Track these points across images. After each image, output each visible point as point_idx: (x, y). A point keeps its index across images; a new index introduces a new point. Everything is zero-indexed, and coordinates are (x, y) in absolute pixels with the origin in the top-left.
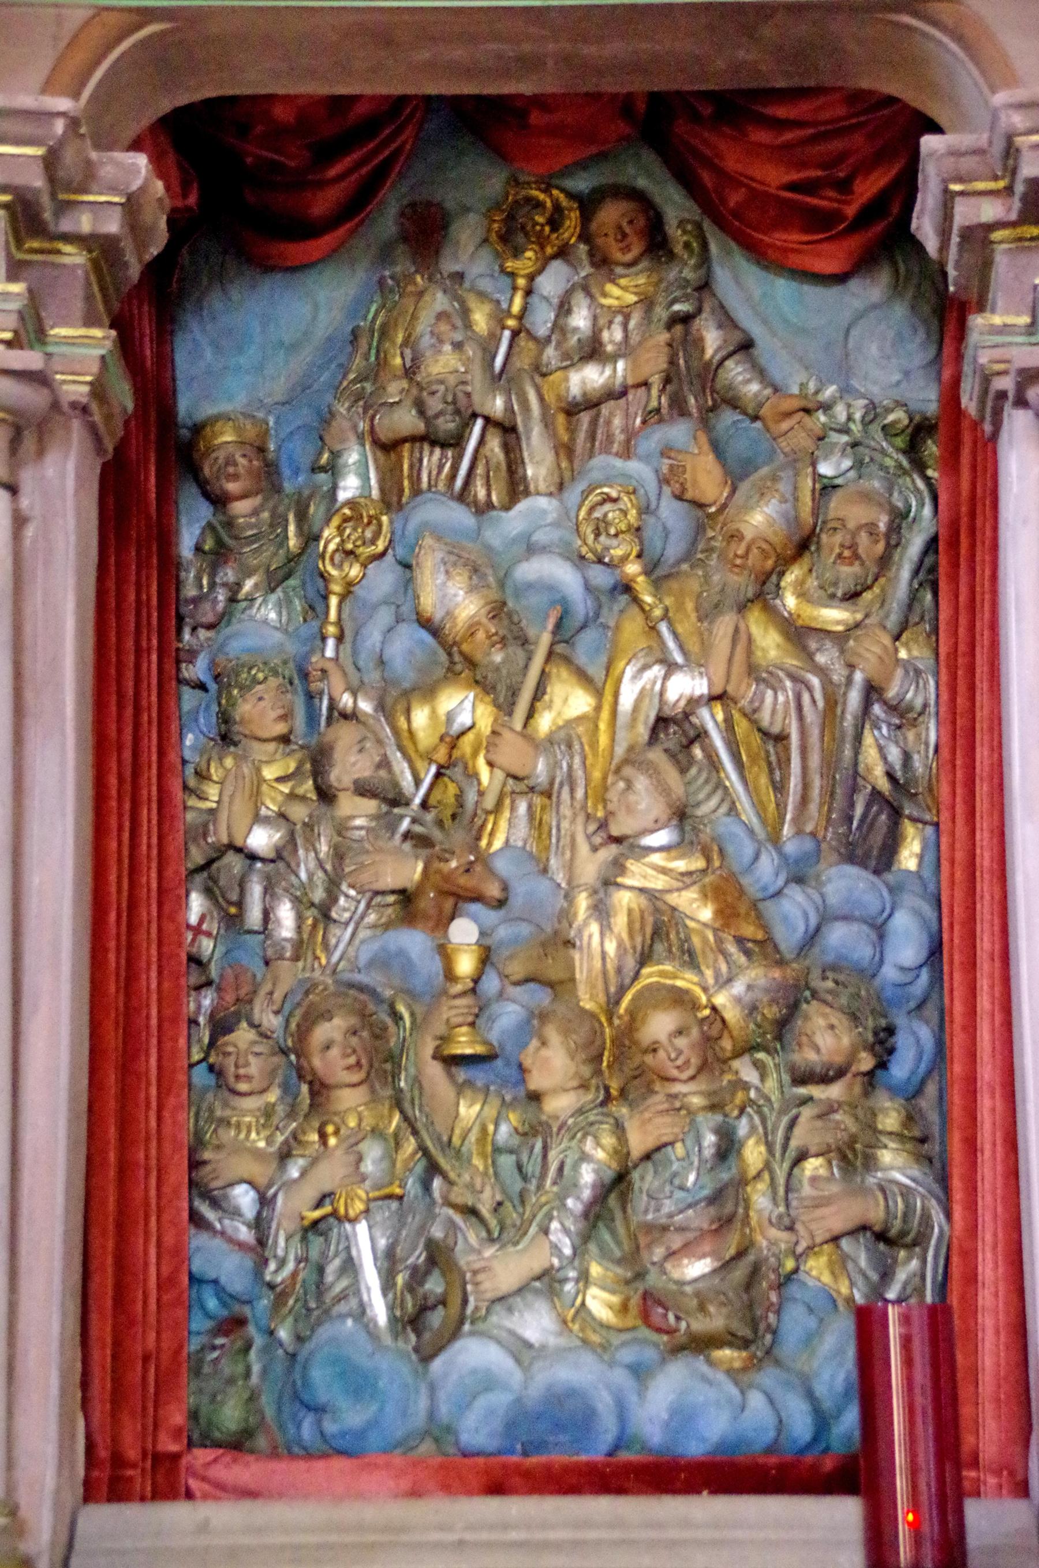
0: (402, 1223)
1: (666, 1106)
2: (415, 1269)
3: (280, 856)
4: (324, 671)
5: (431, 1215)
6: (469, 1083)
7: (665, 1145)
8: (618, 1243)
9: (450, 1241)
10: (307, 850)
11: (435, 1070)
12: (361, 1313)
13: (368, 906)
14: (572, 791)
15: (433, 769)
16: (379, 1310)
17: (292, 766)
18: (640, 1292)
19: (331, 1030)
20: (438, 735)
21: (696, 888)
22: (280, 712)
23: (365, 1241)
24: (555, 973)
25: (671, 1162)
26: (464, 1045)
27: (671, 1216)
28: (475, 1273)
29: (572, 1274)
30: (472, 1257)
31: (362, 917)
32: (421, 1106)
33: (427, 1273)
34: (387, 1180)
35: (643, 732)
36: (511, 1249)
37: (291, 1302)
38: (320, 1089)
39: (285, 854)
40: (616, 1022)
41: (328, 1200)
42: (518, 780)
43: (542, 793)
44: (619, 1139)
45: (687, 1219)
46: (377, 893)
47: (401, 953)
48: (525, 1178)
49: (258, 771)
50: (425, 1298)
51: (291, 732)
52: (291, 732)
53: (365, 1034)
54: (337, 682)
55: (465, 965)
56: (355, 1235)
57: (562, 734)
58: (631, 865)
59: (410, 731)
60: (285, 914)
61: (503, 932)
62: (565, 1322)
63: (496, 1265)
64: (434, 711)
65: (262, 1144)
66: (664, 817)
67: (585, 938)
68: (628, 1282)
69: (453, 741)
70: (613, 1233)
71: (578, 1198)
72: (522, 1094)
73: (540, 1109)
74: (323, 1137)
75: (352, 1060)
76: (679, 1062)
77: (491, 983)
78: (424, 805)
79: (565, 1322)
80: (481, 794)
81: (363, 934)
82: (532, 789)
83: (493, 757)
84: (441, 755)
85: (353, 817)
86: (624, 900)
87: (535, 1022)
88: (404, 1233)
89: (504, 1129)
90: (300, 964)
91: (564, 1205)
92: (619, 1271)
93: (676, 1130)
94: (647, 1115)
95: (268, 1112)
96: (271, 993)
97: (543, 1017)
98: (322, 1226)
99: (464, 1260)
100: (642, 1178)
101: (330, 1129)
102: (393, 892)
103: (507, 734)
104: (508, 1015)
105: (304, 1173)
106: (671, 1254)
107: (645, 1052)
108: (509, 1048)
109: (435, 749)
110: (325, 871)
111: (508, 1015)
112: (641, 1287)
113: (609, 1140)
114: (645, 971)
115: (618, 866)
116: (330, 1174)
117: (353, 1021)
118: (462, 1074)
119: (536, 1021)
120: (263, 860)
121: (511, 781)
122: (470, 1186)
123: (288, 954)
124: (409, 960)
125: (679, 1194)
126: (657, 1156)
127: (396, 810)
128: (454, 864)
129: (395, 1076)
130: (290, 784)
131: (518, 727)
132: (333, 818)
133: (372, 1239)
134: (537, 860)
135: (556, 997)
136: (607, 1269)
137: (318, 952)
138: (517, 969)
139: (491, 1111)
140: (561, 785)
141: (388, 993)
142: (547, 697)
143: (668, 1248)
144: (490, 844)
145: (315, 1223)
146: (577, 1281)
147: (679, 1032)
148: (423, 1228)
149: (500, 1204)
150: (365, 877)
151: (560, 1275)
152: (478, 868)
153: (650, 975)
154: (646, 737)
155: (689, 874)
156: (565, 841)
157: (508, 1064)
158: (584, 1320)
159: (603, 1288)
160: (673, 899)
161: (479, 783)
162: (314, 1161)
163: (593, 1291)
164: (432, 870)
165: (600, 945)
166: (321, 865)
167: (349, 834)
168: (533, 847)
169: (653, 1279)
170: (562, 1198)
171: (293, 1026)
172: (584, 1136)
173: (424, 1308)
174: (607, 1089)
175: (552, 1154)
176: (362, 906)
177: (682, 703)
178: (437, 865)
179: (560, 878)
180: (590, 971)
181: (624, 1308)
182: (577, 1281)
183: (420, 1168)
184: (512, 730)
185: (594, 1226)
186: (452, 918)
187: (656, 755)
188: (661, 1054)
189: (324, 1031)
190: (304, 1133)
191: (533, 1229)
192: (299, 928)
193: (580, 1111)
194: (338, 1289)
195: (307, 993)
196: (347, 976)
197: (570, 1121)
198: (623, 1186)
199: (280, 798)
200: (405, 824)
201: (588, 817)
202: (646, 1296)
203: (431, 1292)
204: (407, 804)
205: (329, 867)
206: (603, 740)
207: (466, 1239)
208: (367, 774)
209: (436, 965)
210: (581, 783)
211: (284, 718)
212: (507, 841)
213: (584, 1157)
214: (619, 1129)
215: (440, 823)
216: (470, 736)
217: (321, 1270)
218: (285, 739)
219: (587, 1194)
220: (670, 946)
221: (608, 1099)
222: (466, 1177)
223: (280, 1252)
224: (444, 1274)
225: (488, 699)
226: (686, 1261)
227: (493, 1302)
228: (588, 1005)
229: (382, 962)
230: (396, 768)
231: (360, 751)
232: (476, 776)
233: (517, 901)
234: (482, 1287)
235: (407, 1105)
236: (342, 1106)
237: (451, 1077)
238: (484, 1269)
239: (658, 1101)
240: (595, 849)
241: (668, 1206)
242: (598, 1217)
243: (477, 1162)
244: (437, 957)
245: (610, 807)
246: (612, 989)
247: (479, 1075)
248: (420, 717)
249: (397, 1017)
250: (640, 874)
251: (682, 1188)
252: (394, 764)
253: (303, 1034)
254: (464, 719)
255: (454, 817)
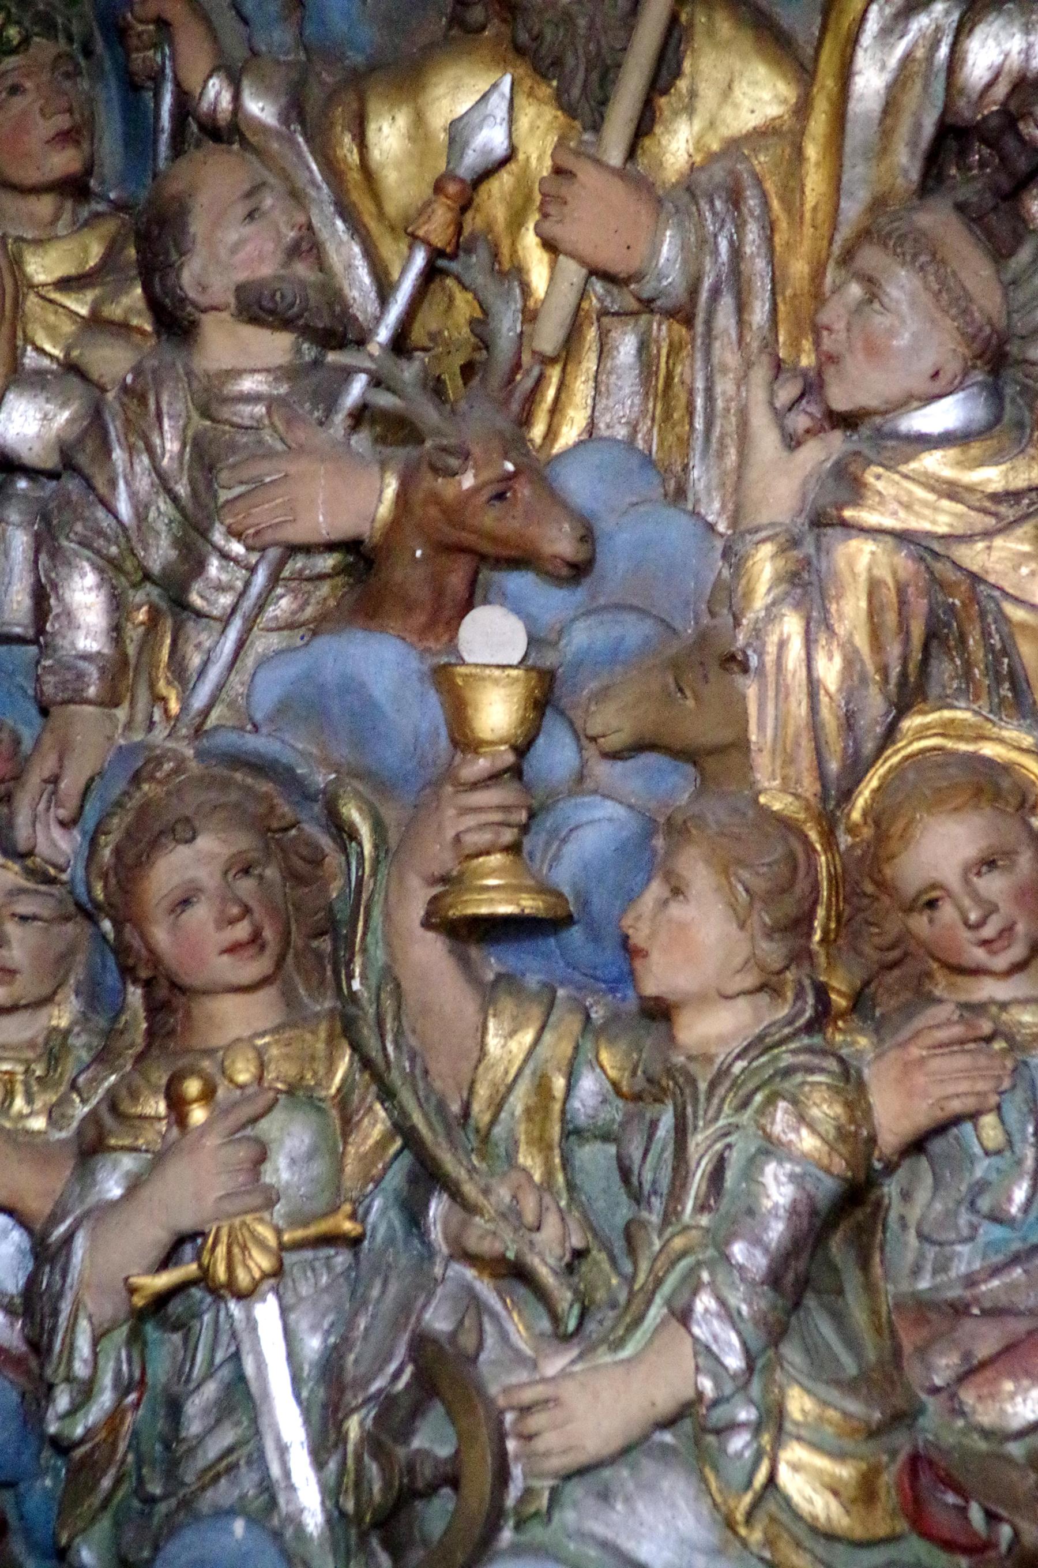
0: (359, 1301)
1: (957, 1031)
2: (387, 1402)
3: (74, 463)
4: (163, 24)
5: (424, 1284)
6: (508, 982)
7: (957, 1120)
8: (852, 1343)
9: (467, 1341)
10: (131, 450)
11: (429, 954)
12: (268, 1503)
13: (274, 579)
14: (741, 308)
15: (420, 259)
16: (308, 1498)
17: (95, 252)
18: (902, 1457)
19: (192, 862)
20: (430, 178)
21: (1026, 528)
22: (63, 121)
23: (272, 1343)
24: (701, 728)
25: (972, 1159)
26: (496, 897)
27: (970, 1281)
28: (525, 1410)
29: (745, 1414)
30: (522, 1376)
31: (260, 607)
32: (399, 1034)
33: (417, 1411)
34: (320, 1204)
35: (905, 161)
36: (604, 1357)
37: (106, 1483)
38: (170, 1000)
39: (82, 459)
40: (845, 840)
41: (188, 1250)
42: (615, 287)
43: (670, 314)
44: (849, 1105)
45: (1012, 1287)
46: (293, 549)
47: (352, 687)
48: (637, 1197)
49: (16, 263)
50: (411, 1469)
51: (89, 170)
52: (89, 170)
53: (271, 873)
54: (192, 54)
55: (496, 713)
56: (252, 1325)
57: (719, 172)
58: (879, 480)
59: (365, 166)
60: (85, 597)
61: (582, 637)
62: (730, 1524)
63: (569, 1390)
64: (419, 120)
65: (38, 1123)
66: (953, 367)
67: (771, 649)
68: (873, 1433)
69: (464, 191)
70: (839, 1318)
71: (756, 1241)
72: (632, 1005)
73: (672, 1039)
74: (178, 1106)
75: (242, 931)
76: (988, 932)
77: (557, 754)
78: (400, 345)
79: (730, 1524)
80: (530, 316)
81: (262, 643)
82: (647, 305)
83: (553, 229)
84: (437, 227)
85: (236, 374)
86: (860, 558)
87: (659, 842)
88: (362, 1323)
89: (588, 1084)
90: (121, 713)
91: (727, 1258)
92: (854, 1406)
93: (981, 1086)
94: (915, 1052)
95: (53, 1049)
96: (54, 780)
97: (677, 829)
98: (176, 1307)
99: (499, 1380)
100: (906, 1196)
101: (193, 1087)
102: (330, 547)
103: (587, 174)
104: (595, 828)
105: (134, 1186)
106: (971, 1371)
107: (909, 909)
108: (598, 903)
109: (424, 210)
110: (175, 499)
111: (595, 828)
112: (902, 1442)
113: (826, 1109)
114: (912, 722)
115: (847, 481)
116: (193, 1188)
117: (243, 842)
118: (492, 963)
119: (655, 845)
120: (32, 473)
121: (598, 286)
122: (512, 1215)
123: (92, 691)
124: (370, 705)
125: (997, 1232)
126: (937, 1146)
127: (332, 357)
128: (468, 481)
129: (341, 966)
130: (90, 295)
131: (615, 157)
132: (189, 373)
133: (289, 1334)
134: (664, 472)
135: (705, 784)
136: (825, 1403)
137: (162, 686)
138: (613, 722)
139: (557, 1046)
140: (716, 293)
141: (322, 778)
142: (683, 84)
143: (967, 1356)
144: (551, 434)
145: (162, 1299)
146: (757, 1429)
147: (988, 863)
148: (405, 1308)
149: (579, 1254)
150: (262, 514)
151: (718, 1416)
152: (524, 491)
153: (921, 733)
154: (915, 175)
155: (1012, 496)
156: (726, 425)
157: (595, 937)
158: (773, 1519)
159: (816, 1447)
160: (974, 556)
161: (526, 290)
162: (159, 1159)
163: (794, 1452)
164: (418, 496)
165: (804, 665)
166: (163, 482)
167: (225, 412)
168: (650, 439)
169: (933, 1420)
170: (719, 1243)
171: (106, 854)
172: (771, 1101)
173: (408, 1493)
174: (822, 991)
175: (697, 1141)
176: (260, 578)
177: (1001, 90)
178: (431, 482)
179: (713, 510)
180: (781, 723)
181: (866, 1492)
182: (757, 1429)
183: (396, 1178)
184: (598, 162)
185: (797, 1305)
186: (468, 605)
187: (937, 219)
188: (947, 912)
189: (174, 867)
190: (134, 1096)
191: (656, 1312)
192: (116, 631)
193: (760, 1044)
194: (213, 1448)
195: (136, 779)
196: (227, 740)
197: (739, 1066)
198: (860, 1215)
199: (68, 327)
200: (358, 386)
201: (778, 367)
202: (916, 1462)
203: (424, 1454)
204: (361, 342)
205: (182, 489)
206: (815, 182)
207: (504, 1337)
208: (266, 270)
209: (428, 713)
210: (761, 286)
211: (66, 137)
212: (592, 425)
213: (771, 1148)
214: (850, 1084)
215: (436, 389)
216: (504, 182)
217: (174, 1408)
218: (75, 188)
219: (776, 1231)
220: (968, 665)
221: (823, 1017)
222: (504, 1193)
223: (81, 1369)
224: (452, 1416)
225: (545, 91)
226: (1009, 1386)
227: (568, 1477)
228: (778, 803)
229: (306, 706)
230: (335, 259)
231: (251, 216)
232: (519, 273)
233: (615, 562)
234: (540, 1444)
235: (368, 1034)
236: (218, 1039)
237: (465, 963)
238: (544, 1403)
239: (940, 1019)
240: (792, 442)
241: (966, 1259)
242: (804, 1284)
243: (528, 1159)
244: (433, 698)
245: (828, 343)
246: (834, 766)
247: (530, 963)
248: (389, 135)
249: (344, 834)
250: (901, 500)
251: (997, 1218)
252: (330, 248)
253: (130, 868)
254: (492, 138)
255: (468, 370)
